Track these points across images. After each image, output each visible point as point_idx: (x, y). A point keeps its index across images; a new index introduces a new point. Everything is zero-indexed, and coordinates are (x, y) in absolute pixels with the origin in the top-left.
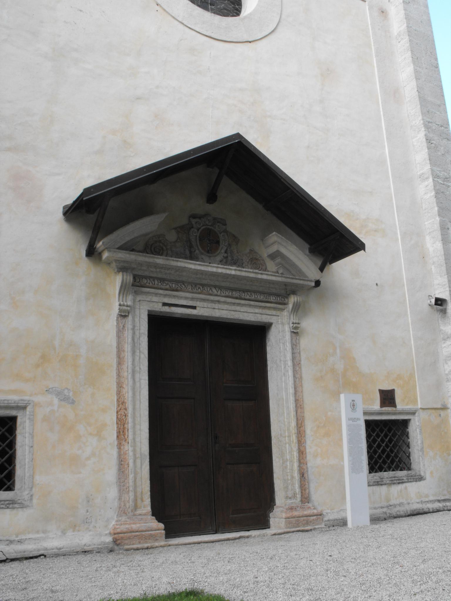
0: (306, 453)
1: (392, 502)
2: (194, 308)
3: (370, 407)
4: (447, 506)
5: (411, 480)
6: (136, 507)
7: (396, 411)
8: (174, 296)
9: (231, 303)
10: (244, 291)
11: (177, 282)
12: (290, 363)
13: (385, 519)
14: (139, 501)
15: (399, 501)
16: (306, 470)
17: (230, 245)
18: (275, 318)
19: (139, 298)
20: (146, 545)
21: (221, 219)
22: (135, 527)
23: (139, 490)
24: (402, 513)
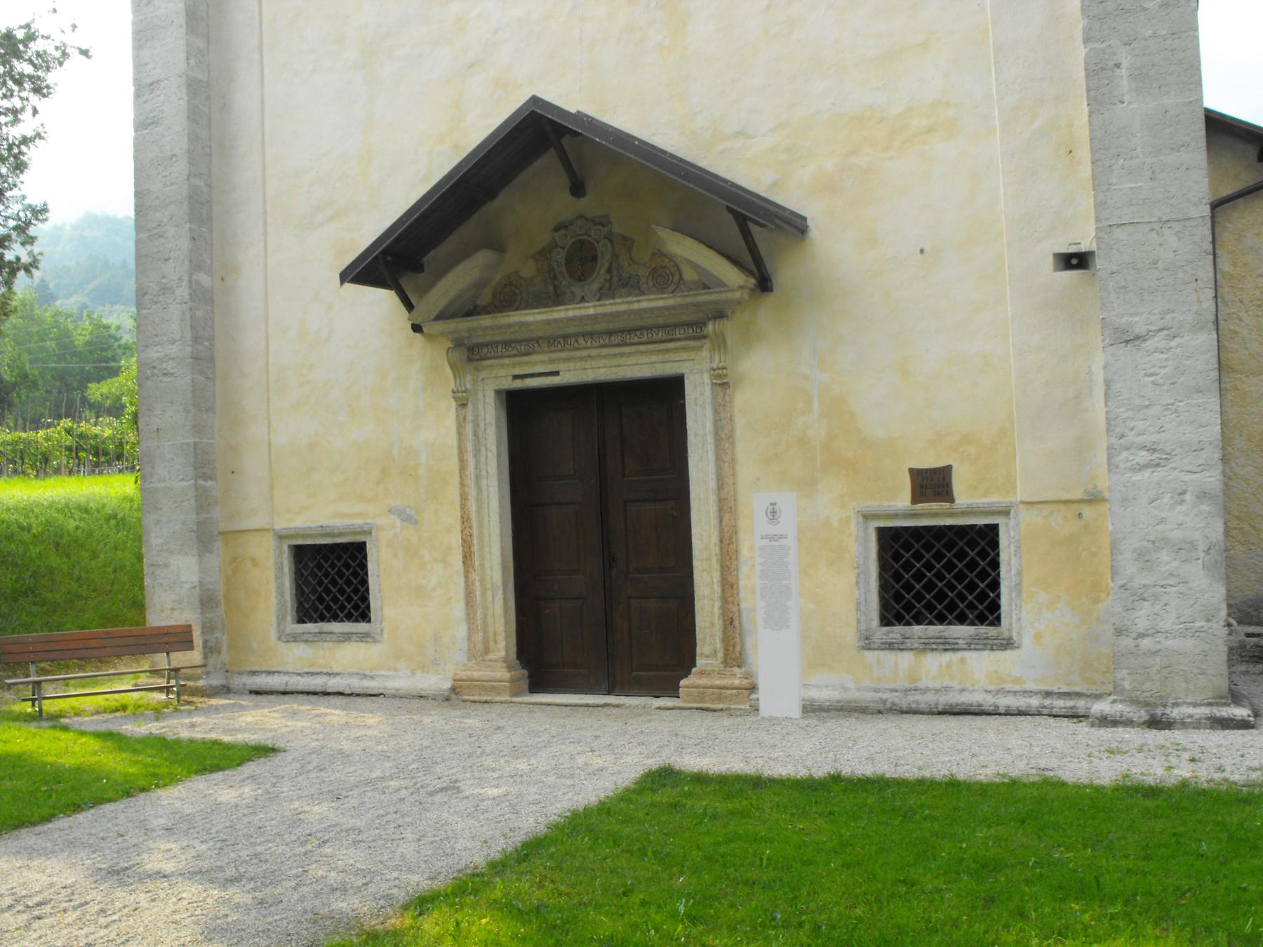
0: (738, 587)
1: (920, 685)
2: (556, 373)
3: (886, 503)
4: (1052, 708)
5: (977, 647)
6: (487, 650)
7: (951, 510)
8: (526, 364)
9: (609, 355)
10: (629, 331)
11: (528, 341)
12: (710, 439)
13: (880, 712)
14: (491, 643)
15: (942, 683)
16: (736, 615)
17: (615, 257)
18: (688, 364)
19: (483, 375)
20: (484, 698)
21: (602, 216)
22: (476, 674)
23: (491, 629)
24: (923, 706)
